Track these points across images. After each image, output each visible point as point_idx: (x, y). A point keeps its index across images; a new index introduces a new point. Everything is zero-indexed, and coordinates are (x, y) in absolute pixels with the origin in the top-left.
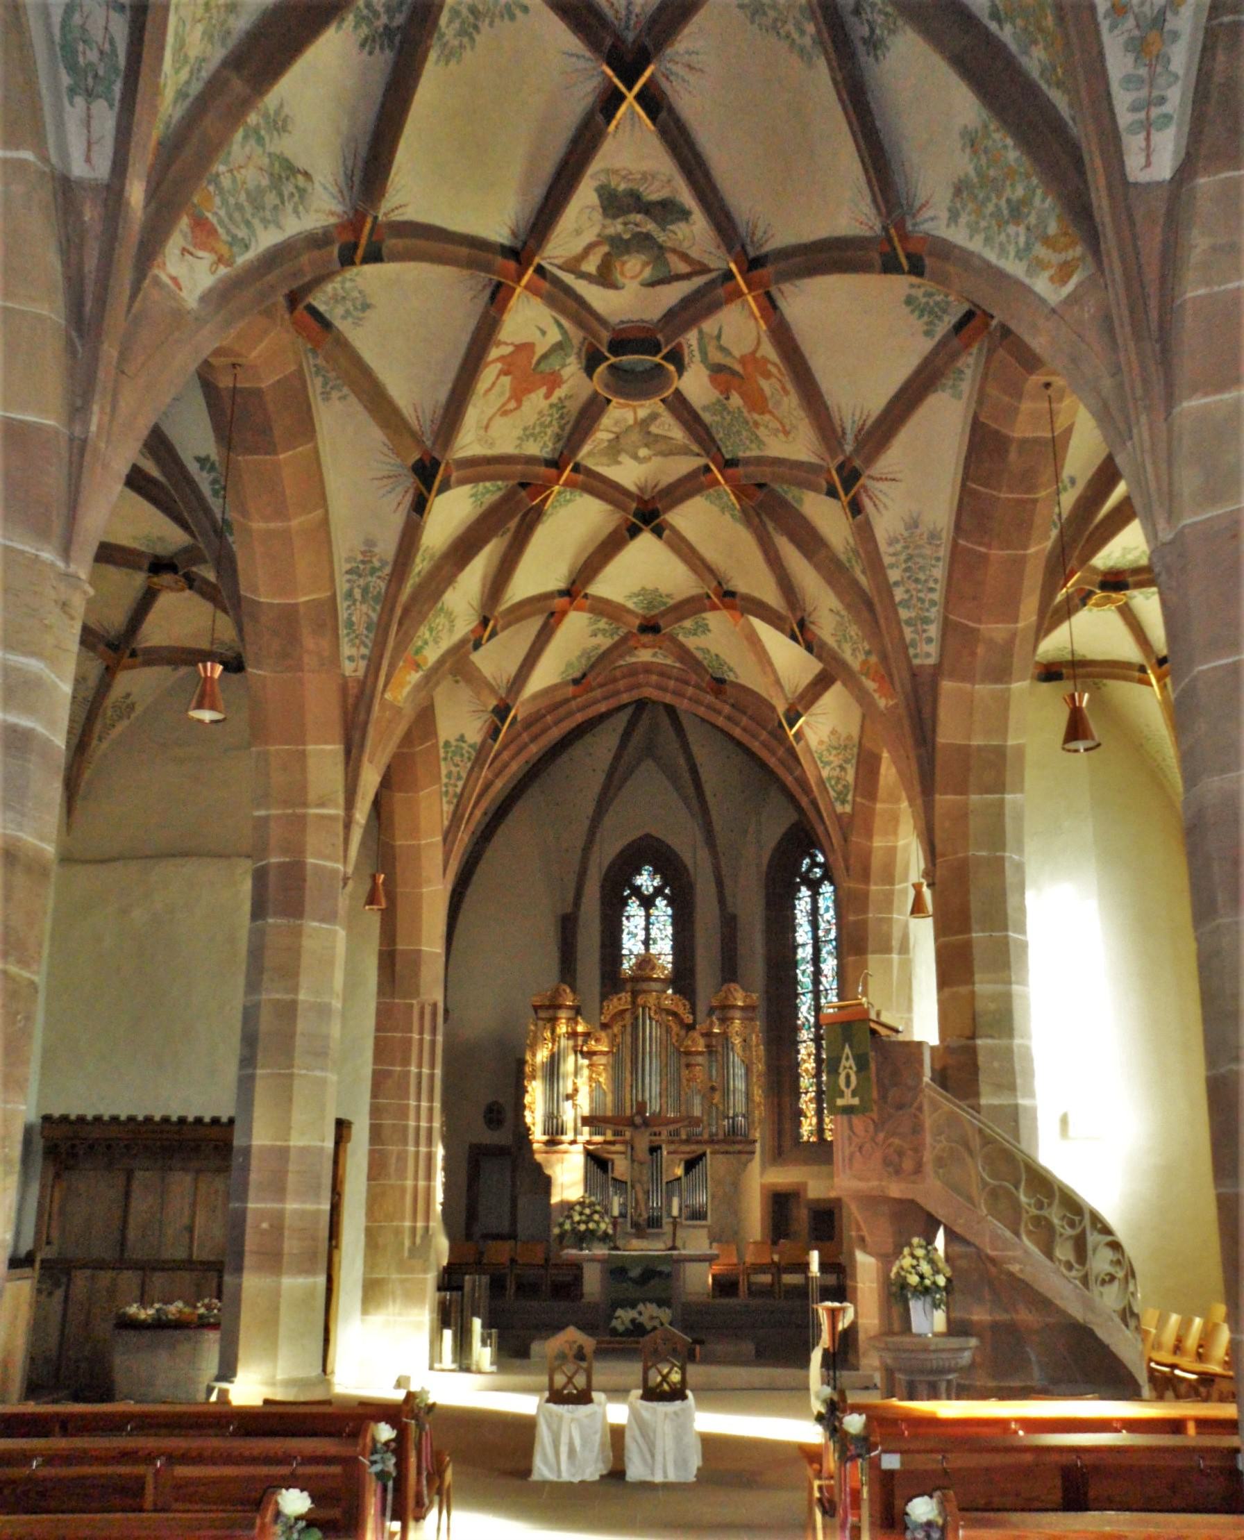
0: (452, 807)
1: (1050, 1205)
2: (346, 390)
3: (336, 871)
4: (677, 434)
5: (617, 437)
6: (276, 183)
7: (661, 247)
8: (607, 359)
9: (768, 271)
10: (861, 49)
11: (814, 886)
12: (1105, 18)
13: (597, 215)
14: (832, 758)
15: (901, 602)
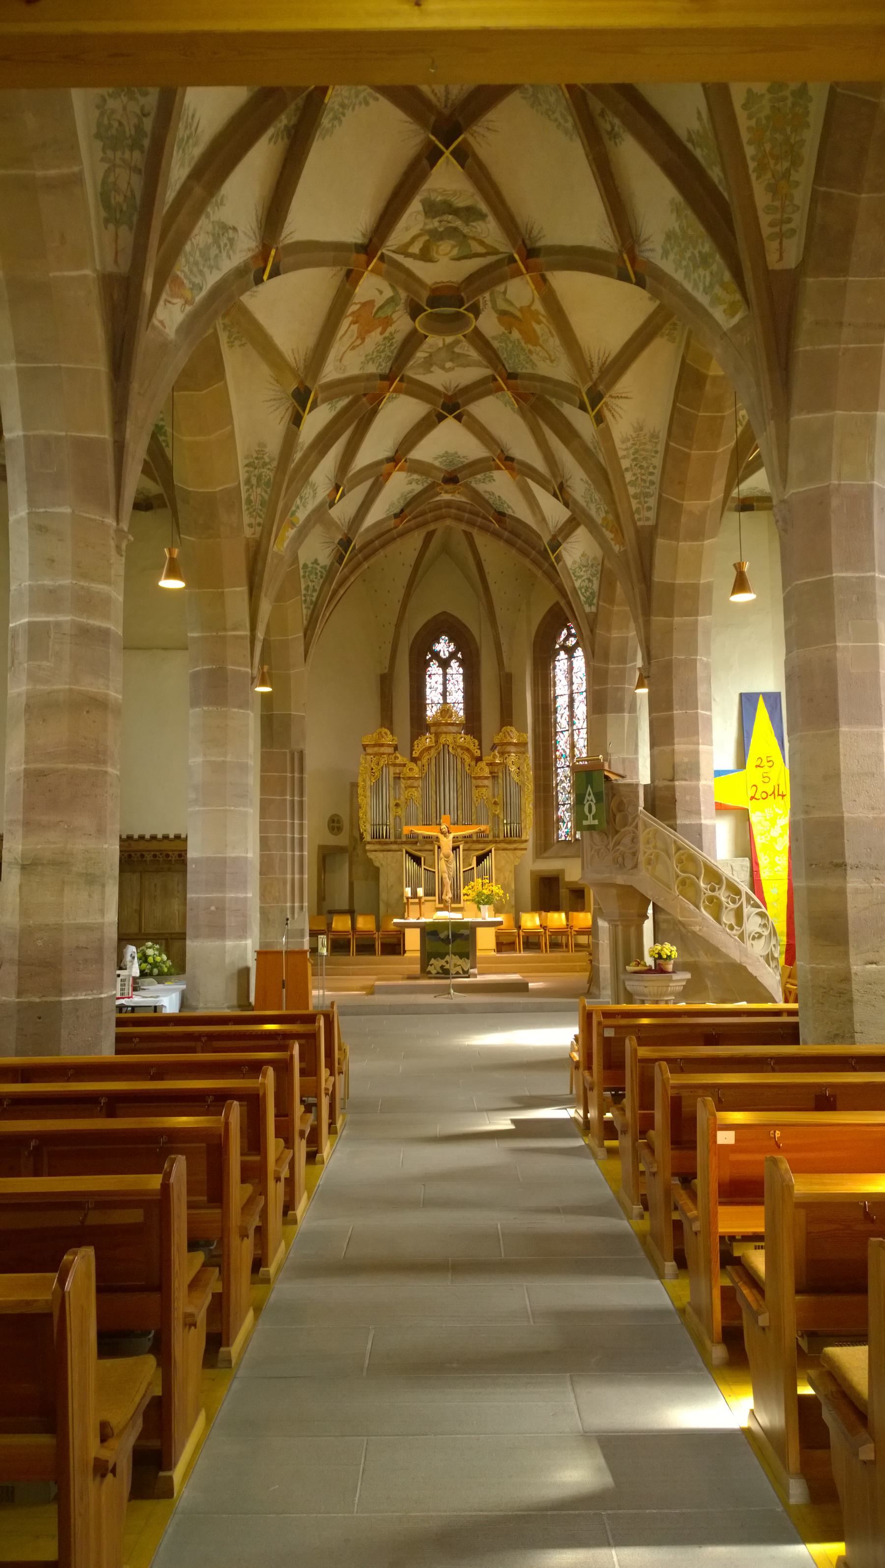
0: (310, 611)
1: (719, 889)
2: (244, 340)
3: (247, 673)
4: (474, 354)
5: (431, 355)
6: (216, 239)
7: (465, 236)
8: (425, 310)
9: (541, 260)
10: (606, 137)
11: (570, 651)
12: (753, 171)
13: (421, 217)
14: (582, 573)
15: (629, 482)
